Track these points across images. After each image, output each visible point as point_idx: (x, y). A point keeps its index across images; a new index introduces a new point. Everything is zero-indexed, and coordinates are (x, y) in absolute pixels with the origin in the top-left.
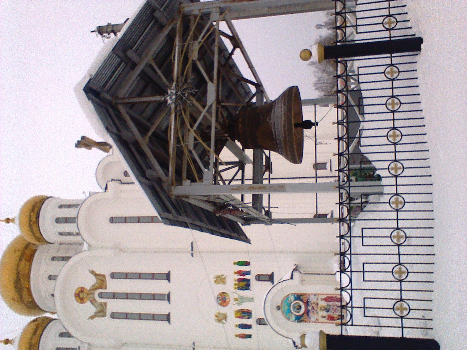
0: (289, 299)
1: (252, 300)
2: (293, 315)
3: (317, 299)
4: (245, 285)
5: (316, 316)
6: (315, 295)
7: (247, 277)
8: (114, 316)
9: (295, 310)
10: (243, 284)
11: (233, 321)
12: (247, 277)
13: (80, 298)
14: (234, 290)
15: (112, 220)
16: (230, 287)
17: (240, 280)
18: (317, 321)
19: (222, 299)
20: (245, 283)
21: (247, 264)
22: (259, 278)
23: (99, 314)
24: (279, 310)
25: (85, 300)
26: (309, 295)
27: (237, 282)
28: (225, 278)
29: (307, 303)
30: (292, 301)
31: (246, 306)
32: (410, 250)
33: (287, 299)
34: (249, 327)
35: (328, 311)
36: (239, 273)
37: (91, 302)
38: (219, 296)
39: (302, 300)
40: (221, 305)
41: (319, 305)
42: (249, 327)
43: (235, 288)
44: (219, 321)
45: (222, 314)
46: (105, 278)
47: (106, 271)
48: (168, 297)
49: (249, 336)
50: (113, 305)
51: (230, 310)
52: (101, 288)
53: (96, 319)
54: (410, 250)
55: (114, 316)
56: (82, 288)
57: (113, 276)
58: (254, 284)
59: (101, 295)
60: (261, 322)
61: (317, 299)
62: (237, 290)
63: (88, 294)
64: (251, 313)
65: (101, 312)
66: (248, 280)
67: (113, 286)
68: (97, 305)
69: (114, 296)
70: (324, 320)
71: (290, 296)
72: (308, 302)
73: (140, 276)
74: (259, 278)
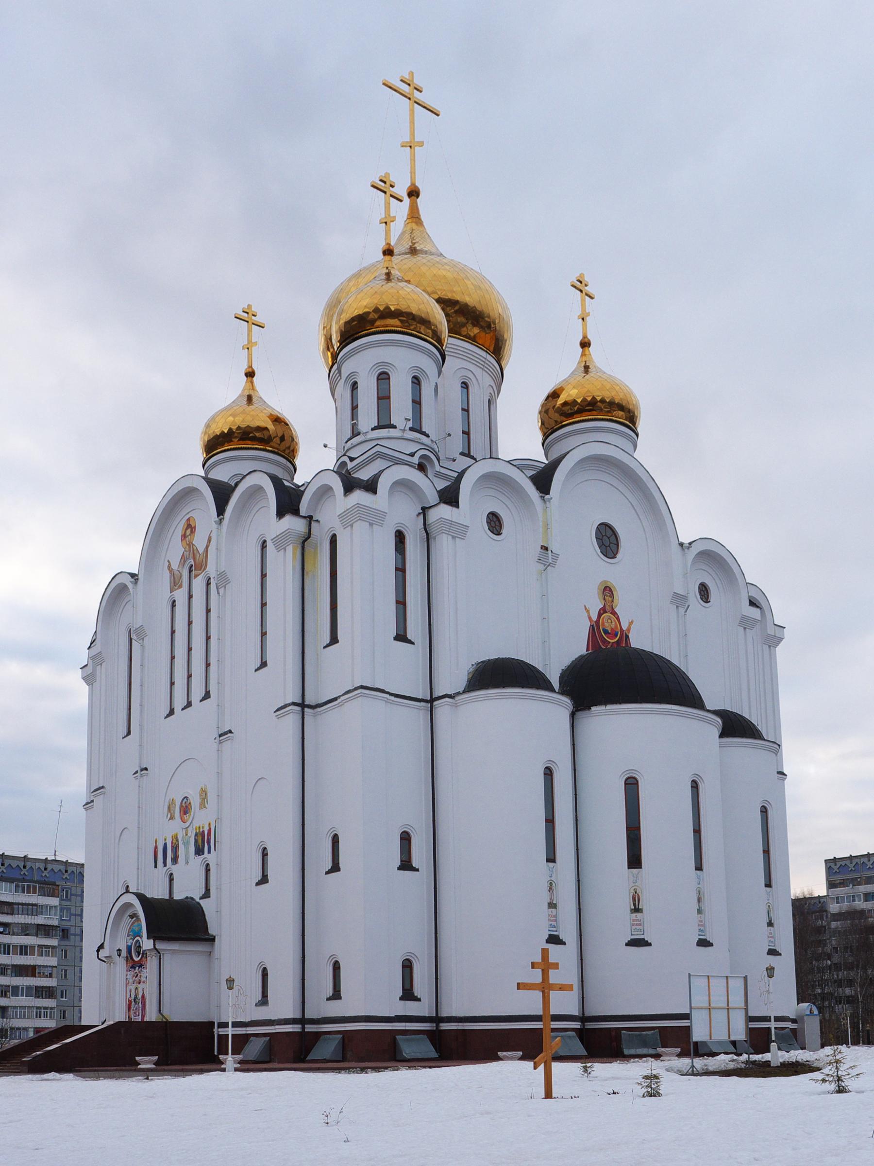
65: (175, 584)
68: (180, 569)
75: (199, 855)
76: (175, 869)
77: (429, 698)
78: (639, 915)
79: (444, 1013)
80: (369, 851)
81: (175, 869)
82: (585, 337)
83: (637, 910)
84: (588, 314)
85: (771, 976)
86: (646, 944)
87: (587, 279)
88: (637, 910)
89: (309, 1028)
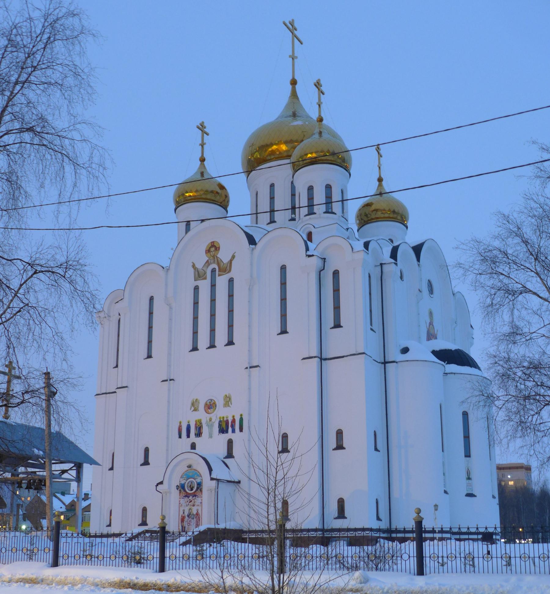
0: (198, 477)
1: (211, 436)
2: (185, 481)
3: (198, 505)
4: (223, 428)
5: (184, 504)
6: (201, 503)
7: (230, 429)
8: (196, 288)
9: (190, 484)
10: (224, 425)
11: (192, 418)
12: (230, 429)
13: (210, 248)
14: (218, 417)
15: (283, 268)
16: (222, 412)
17: (227, 422)
18: (180, 505)
19: (211, 405)
20: (225, 429)
21: (241, 430)
22: (230, 443)
23: (197, 273)
24: (188, 467)
25: (209, 254)
26: (202, 497)
27: (225, 419)
28: (229, 406)
29: (194, 495)
30: (197, 480)
31: (205, 430)
32: (10, 554)
33: (198, 475)
34: (188, 436)
35: (188, 516)
36: (234, 421)
37: (208, 261)
38: (213, 402)
39: (197, 490)
40: (206, 404)
41: (193, 507)
42: (188, 436)
43: (220, 418)
44: (193, 404)
45: (198, 407)
46: (228, 273)
47: (233, 274)
48: (212, 346)
49: (180, 437)
50: (205, 286)
51: (202, 415)
52: (220, 271)
53: (192, 270)
54: (10, 554)
55: (196, 288)
56: (219, 248)
57: (231, 281)
58: (225, 437)
59: (213, 271)
60: (193, 446)
61: (198, 505)
62: (218, 420)
63: (213, 256)
64: (200, 436)
65: (199, 275)
66: (227, 432)
67: (222, 282)
68: (204, 269)
69: (213, 286)
70: (181, 513)
71: (200, 478)
72: (195, 496)
73: (231, 311)
74: (230, 443)
75: (223, 433)
76: (198, 441)
77: (383, 361)
78: (470, 481)
79: (393, 527)
80: (358, 440)
81: (198, 441)
82: (380, 176)
83: (469, 478)
84: (205, 144)
85: (436, 510)
86: (475, 496)
87: (205, 124)
88: (469, 478)
89: (327, 535)
